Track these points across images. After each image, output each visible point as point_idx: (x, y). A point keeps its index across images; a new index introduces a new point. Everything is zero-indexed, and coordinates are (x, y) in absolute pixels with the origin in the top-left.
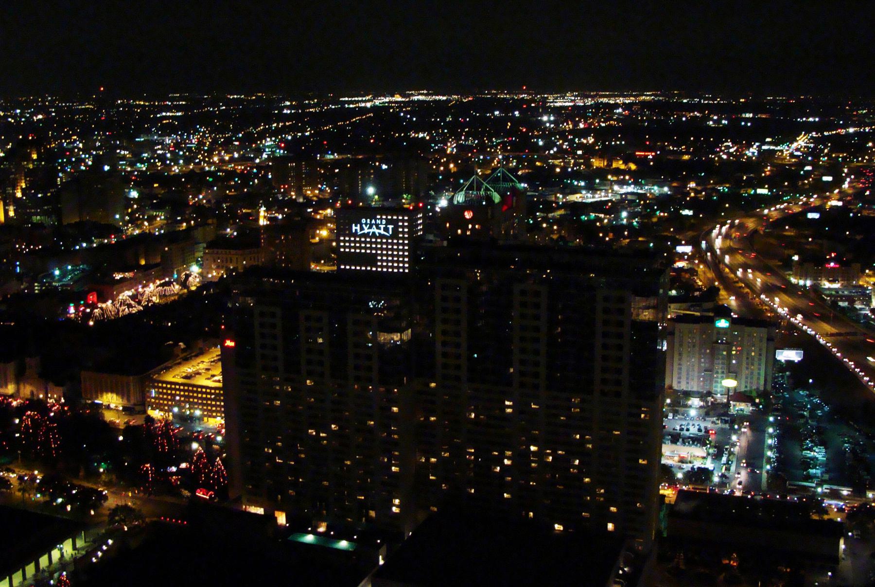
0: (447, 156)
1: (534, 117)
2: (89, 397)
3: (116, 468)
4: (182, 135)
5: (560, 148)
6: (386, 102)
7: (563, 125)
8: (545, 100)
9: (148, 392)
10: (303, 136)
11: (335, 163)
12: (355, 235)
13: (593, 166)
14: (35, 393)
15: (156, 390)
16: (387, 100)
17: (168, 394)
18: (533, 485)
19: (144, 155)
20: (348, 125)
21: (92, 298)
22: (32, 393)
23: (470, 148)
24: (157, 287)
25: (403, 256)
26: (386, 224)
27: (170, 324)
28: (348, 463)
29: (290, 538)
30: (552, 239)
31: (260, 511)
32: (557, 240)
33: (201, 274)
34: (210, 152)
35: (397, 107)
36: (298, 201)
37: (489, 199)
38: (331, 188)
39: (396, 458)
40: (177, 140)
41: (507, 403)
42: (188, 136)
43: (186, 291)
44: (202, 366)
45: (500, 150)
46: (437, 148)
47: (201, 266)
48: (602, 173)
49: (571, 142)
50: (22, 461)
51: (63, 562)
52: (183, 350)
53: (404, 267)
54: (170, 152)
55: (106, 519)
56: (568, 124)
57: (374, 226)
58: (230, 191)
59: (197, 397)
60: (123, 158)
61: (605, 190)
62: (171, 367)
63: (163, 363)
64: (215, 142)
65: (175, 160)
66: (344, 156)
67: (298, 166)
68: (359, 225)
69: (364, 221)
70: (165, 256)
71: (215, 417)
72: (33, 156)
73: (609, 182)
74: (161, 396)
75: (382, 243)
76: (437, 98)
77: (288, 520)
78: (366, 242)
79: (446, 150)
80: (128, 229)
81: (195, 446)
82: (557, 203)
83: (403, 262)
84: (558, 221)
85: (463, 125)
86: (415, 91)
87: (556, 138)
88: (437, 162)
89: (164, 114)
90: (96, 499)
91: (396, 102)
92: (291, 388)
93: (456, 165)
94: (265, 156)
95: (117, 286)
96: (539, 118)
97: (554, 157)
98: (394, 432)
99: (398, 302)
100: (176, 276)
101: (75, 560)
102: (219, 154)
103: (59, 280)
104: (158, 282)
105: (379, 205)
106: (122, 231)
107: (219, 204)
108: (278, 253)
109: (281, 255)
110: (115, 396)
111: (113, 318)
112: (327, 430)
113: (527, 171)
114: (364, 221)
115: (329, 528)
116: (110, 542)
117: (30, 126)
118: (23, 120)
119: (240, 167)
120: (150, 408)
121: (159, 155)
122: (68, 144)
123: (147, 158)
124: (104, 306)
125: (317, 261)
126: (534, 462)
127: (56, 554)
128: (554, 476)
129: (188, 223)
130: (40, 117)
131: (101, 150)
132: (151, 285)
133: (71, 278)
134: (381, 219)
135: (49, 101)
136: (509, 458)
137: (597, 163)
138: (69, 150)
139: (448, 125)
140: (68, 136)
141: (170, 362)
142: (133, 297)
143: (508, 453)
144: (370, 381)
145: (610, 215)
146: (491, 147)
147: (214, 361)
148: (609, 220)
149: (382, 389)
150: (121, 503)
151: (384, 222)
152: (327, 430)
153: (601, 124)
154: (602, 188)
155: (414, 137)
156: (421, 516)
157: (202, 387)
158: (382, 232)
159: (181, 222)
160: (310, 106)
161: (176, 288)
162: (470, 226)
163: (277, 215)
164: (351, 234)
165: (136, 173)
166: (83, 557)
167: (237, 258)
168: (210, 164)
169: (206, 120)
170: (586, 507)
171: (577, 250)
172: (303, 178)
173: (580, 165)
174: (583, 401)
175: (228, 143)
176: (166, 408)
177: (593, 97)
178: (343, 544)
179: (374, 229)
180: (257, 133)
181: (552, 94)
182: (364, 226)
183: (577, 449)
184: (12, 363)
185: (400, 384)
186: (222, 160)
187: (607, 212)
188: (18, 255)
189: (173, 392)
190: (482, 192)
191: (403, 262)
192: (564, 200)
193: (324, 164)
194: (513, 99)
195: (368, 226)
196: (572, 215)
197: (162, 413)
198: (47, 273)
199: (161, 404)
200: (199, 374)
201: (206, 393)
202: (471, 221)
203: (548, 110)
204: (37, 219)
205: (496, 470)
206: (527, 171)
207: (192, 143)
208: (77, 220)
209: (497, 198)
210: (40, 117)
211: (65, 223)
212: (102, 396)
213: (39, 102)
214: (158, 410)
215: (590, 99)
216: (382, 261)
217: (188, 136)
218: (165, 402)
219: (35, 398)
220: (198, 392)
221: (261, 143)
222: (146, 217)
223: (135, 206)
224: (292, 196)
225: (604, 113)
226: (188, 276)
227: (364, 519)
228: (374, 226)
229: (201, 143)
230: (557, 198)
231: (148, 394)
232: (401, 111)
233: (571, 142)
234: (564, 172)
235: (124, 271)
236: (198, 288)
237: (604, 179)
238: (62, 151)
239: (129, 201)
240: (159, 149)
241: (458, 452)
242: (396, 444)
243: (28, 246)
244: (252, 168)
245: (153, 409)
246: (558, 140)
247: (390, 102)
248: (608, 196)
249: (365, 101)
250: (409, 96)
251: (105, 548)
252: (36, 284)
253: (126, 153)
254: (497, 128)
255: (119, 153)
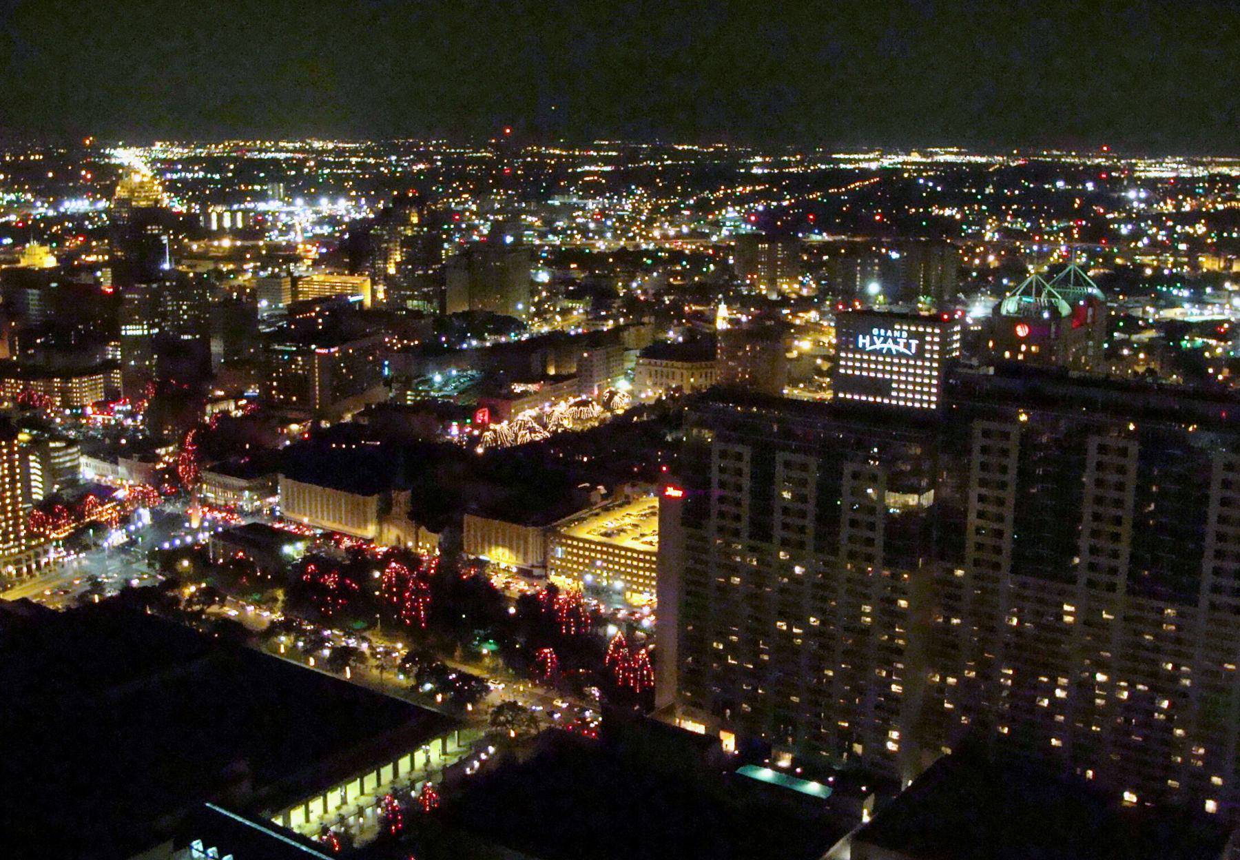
0: (984, 244)
1: (1116, 192)
2: (472, 549)
3: (505, 651)
4: (611, 198)
5: (1153, 239)
6: (899, 163)
7: (1158, 204)
8: (1132, 168)
9: (552, 550)
10: (779, 206)
11: (824, 247)
12: (862, 351)
13: (1202, 268)
14: (402, 539)
15: (564, 548)
16: (901, 159)
17: (585, 557)
18: (1096, 731)
19: (558, 223)
20: (843, 194)
21: (482, 416)
22: (398, 539)
23: (1019, 235)
24: (570, 406)
25: (930, 385)
26: (908, 338)
27: (585, 459)
28: (831, 673)
29: (740, 771)
30: (1136, 373)
31: (700, 729)
32: (1143, 374)
33: (631, 393)
34: (650, 222)
35: (915, 171)
36: (769, 298)
37: (1054, 310)
38: (818, 282)
39: (899, 673)
40: (604, 205)
41: (1067, 608)
42: (620, 200)
43: (609, 414)
44: (628, 520)
45: (1063, 238)
46: (970, 231)
47: (632, 381)
48: (1215, 280)
49: (1171, 230)
50: (382, 627)
51: (429, 769)
52: (604, 497)
53: (928, 399)
54: (594, 220)
55: (488, 717)
56: (1166, 203)
57: (890, 340)
58: (675, 279)
59: (617, 563)
60: (530, 227)
61: (1220, 304)
62: (584, 519)
63: (575, 512)
64: (656, 209)
65: (601, 233)
66: (837, 238)
67: (772, 251)
68: (868, 337)
69: (875, 331)
70: (581, 363)
71: (641, 592)
72: (412, 219)
73: (1227, 293)
74: (570, 557)
75: (900, 365)
76: (973, 159)
77: (737, 745)
78: (876, 362)
79: (983, 236)
80: (533, 325)
81: (612, 630)
82: (1146, 320)
83: (929, 394)
84: (1149, 347)
85: (1009, 201)
86: (940, 147)
87: (1147, 225)
88: (970, 251)
89: (587, 168)
90: (473, 689)
91: (913, 163)
92: (757, 560)
93: (998, 257)
94: (725, 232)
95: (514, 403)
96: (1123, 194)
97: (1144, 253)
98: (900, 636)
99: (918, 451)
100: (596, 392)
101: (445, 770)
102: (661, 227)
103: (440, 390)
104: (572, 400)
105: (884, 309)
106: (524, 327)
107: (658, 296)
108: (740, 369)
109: (743, 373)
110: (507, 551)
111: (509, 445)
112: (802, 622)
113: (1102, 271)
114: (875, 331)
115: (795, 763)
116: (491, 749)
117: (409, 179)
118: (399, 169)
119: (689, 247)
120: (553, 573)
121: (578, 225)
122: (457, 204)
123: (562, 228)
124: (497, 427)
125: (794, 383)
126: (1100, 697)
127: (420, 757)
128: (1127, 721)
129: (616, 320)
130: (422, 166)
131: (500, 214)
132: (562, 403)
133: (456, 388)
134: (901, 330)
135: (434, 146)
136: (1063, 688)
137: (1208, 263)
138: (458, 213)
139: (987, 199)
140: (457, 194)
141: (584, 511)
142: (538, 419)
143: (1063, 681)
144: (869, 559)
145: (1226, 342)
146: (1050, 234)
147: (645, 515)
148: (1224, 349)
149: (887, 573)
150: (509, 698)
151: (905, 334)
152: (802, 622)
153: (1217, 205)
154: (1216, 301)
155: (937, 215)
156: (928, 761)
157: (627, 549)
158: (901, 349)
159: (605, 318)
160: (788, 164)
161: (597, 410)
162: (1023, 348)
163: (739, 316)
164: (857, 350)
165: (547, 248)
166: (455, 765)
167: (682, 374)
168: (646, 238)
169: (645, 179)
170: (1173, 771)
171: (1174, 391)
172: (778, 266)
173: (1182, 265)
174: (1180, 615)
175: (674, 210)
176: (576, 574)
177: (1204, 165)
178: (813, 788)
179: (890, 344)
180: (715, 199)
181: (1143, 159)
182: (875, 338)
183: (1164, 685)
184: (376, 497)
185: (912, 568)
186: (665, 237)
187: (1222, 337)
188: (388, 351)
189: (593, 554)
190: (1044, 299)
191: (929, 394)
192: (1157, 317)
193: (808, 249)
194: (1084, 164)
195: (882, 339)
196: (1168, 338)
197: (570, 581)
198: (422, 378)
199: (569, 569)
200: (623, 531)
201: (632, 558)
202: (1027, 340)
203: (1135, 183)
204: (412, 304)
205: (1041, 704)
206: (1102, 271)
207: (624, 210)
208: (466, 308)
209: (1065, 309)
210: (422, 166)
211: (449, 312)
212: (490, 551)
213: (421, 146)
214: (564, 577)
215: (1201, 168)
216: (898, 390)
217: (620, 200)
218: (575, 566)
219: (402, 546)
220: (620, 556)
221: (720, 213)
222: (558, 309)
223: (544, 294)
224: (761, 290)
225: (1222, 190)
226: (612, 394)
227: (845, 755)
228: (890, 340)
229: (637, 211)
230: (1145, 312)
231: (552, 553)
232: (920, 176)
233: (1171, 230)
234: (1158, 278)
235: (527, 381)
236: (626, 411)
237: (1218, 286)
238: (449, 214)
239: (534, 288)
240: (578, 216)
241: (987, 672)
242: (899, 651)
243: (400, 340)
244: (706, 248)
245: (557, 574)
246: (1150, 227)
247: (904, 163)
248: (1222, 314)
249: (869, 160)
250: (932, 154)
251: (483, 756)
252: (409, 393)
253: (534, 219)
254: (1061, 207)
255: (525, 219)
